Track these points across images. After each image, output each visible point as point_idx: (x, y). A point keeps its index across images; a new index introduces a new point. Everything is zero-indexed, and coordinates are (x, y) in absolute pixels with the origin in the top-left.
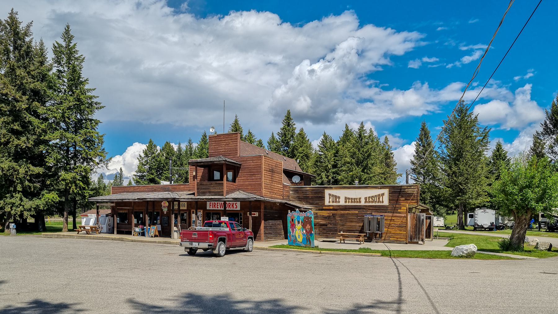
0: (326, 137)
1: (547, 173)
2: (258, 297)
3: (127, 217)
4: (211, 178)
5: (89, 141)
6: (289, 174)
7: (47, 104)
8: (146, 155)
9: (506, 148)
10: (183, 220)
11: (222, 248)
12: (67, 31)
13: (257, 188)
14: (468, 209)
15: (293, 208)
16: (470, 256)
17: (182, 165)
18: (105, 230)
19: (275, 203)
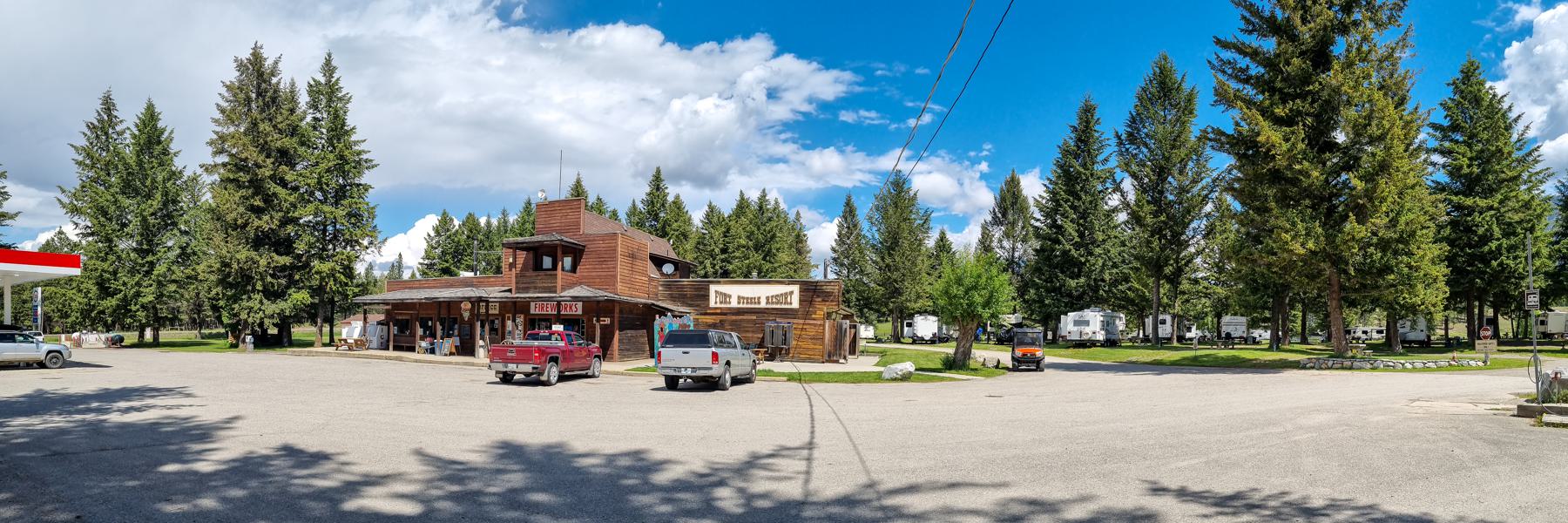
0: (712, 208)
1: (994, 271)
2: (610, 448)
3: (408, 326)
4: (538, 266)
5: (355, 216)
6: (658, 261)
7: (298, 167)
8: (438, 233)
9: (950, 237)
10: (493, 330)
11: (553, 372)
12: (328, 62)
13: (610, 281)
14: (905, 316)
15: (663, 312)
16: (906, 378)
17: (491, 247)
18: (375, 344)
19: (636, 304)
